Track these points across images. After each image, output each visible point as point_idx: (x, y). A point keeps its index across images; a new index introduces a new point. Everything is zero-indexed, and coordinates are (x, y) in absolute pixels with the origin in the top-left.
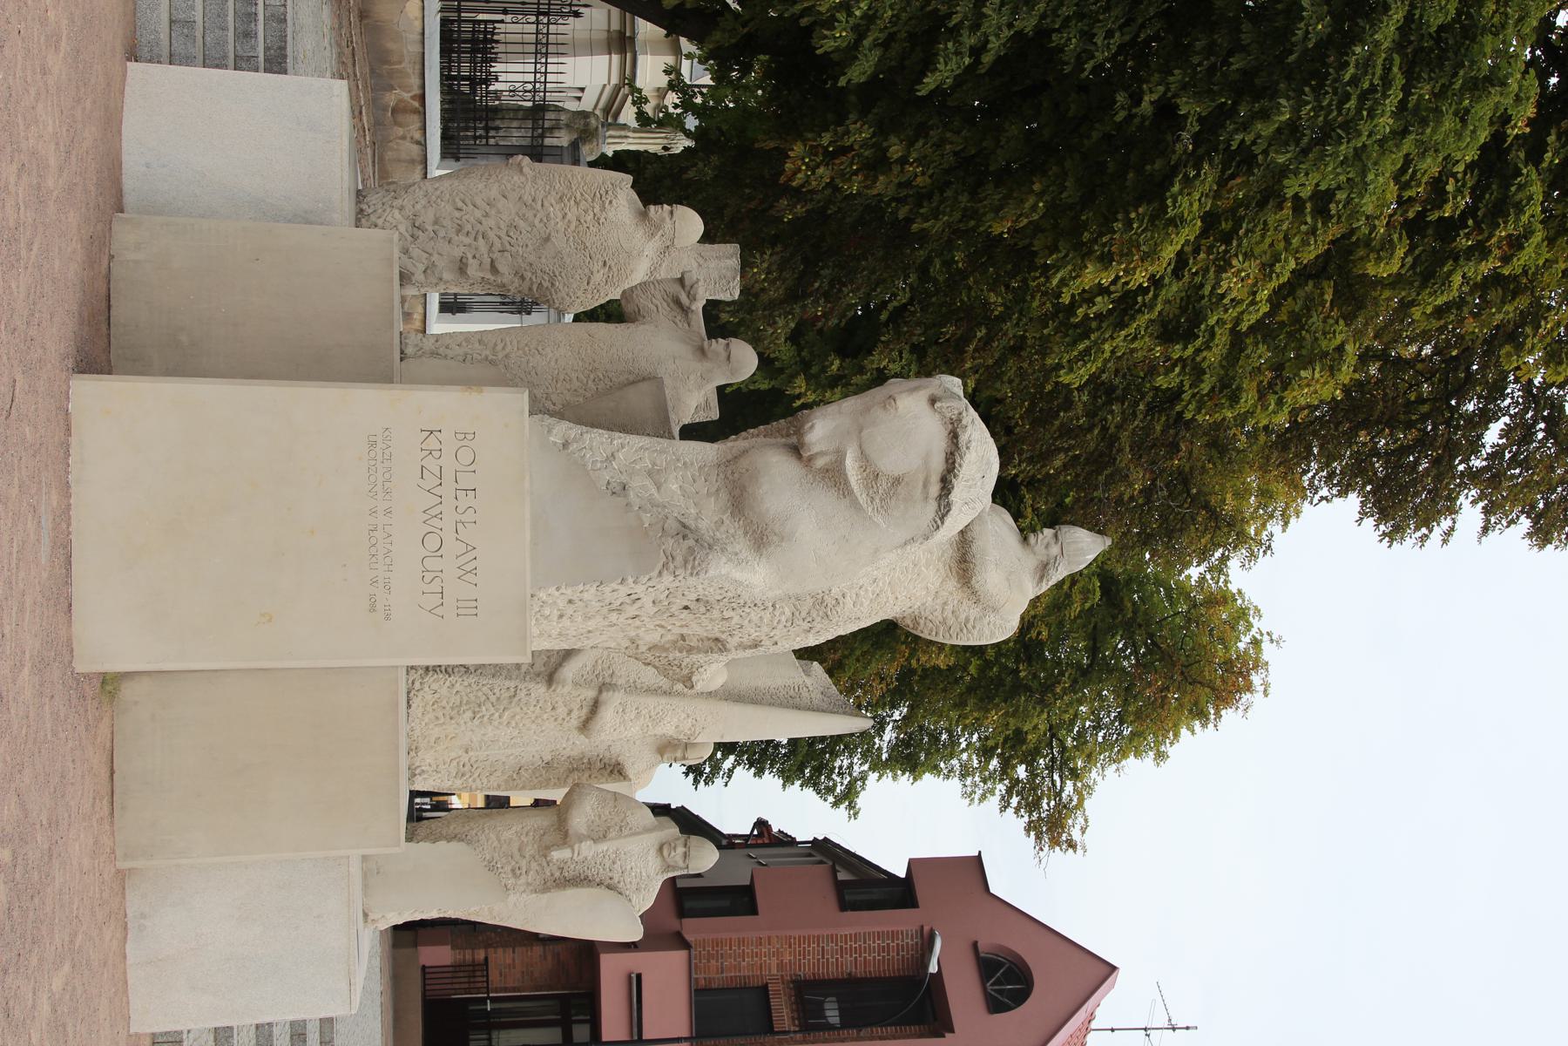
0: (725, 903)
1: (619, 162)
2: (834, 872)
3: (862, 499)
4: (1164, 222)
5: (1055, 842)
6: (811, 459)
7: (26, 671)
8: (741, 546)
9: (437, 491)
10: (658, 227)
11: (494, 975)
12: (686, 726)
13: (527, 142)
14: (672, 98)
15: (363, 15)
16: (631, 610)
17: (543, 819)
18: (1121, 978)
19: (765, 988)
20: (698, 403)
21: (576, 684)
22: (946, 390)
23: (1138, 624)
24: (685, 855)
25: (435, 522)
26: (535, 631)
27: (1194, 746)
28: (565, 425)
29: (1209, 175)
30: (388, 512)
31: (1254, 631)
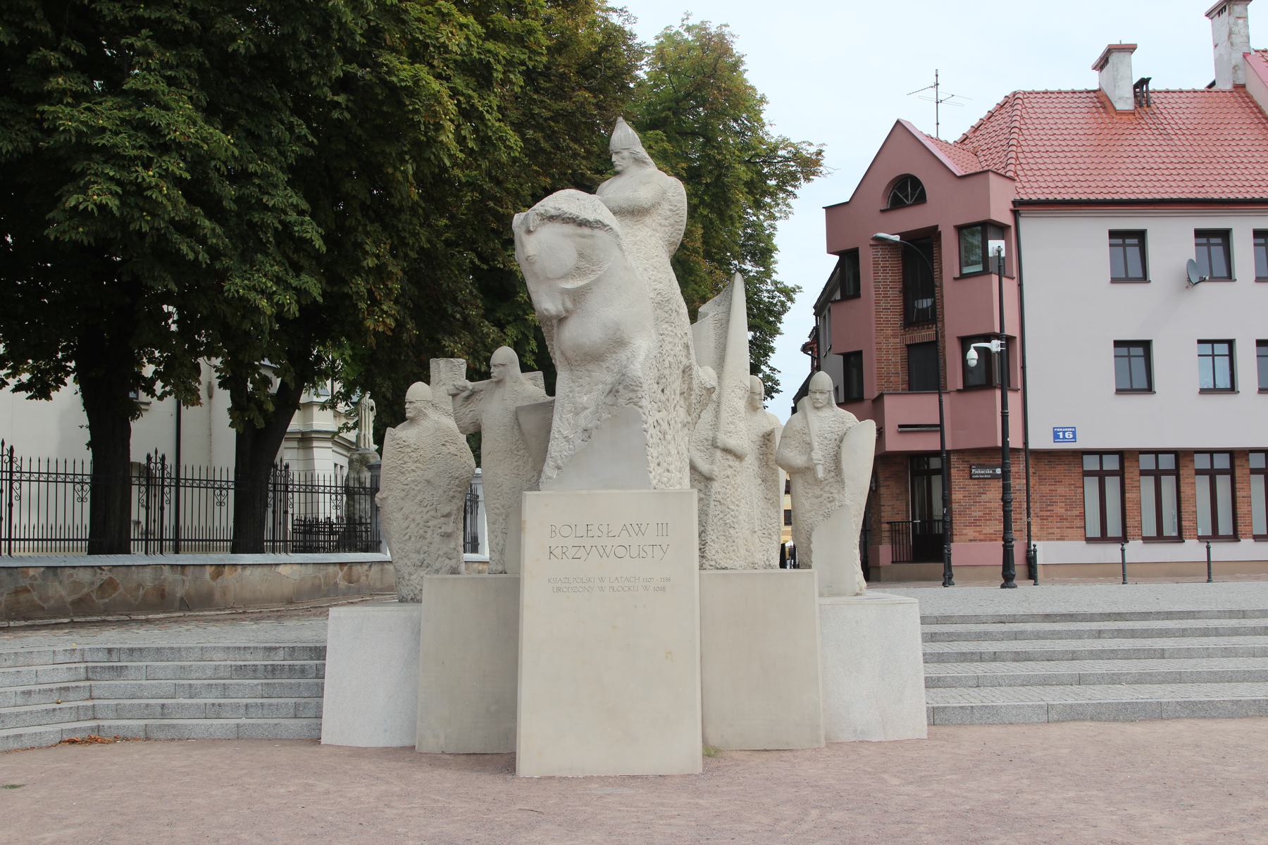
0: (854, 371)
1: (379, 439)
2: (836, 301)
3: (592, 277)
4: (414, 89)
5: (817, 163)
6: (567, 311)
7: (701, 802)
8: (623, 356)
9: (588, 549)
10: (420, 411)
11: (898, 518)
12: (740, 393)
13: (368, 498)
14: (341, 407)
15: (290, 602)
16: (665, 426)
17: (798, 486)
18: (904, 118)
19: (908, 346)
20: (532, 385)
21: (712, 463)
22: (522, 223)
23: (677, 105)
24: (822, 392)
25: (608, 550)
26: (678, 487)
27: (755, 75)
28: (546, 468)
29: (387, 58)
30: (602, 580)
31: (681, 30)
